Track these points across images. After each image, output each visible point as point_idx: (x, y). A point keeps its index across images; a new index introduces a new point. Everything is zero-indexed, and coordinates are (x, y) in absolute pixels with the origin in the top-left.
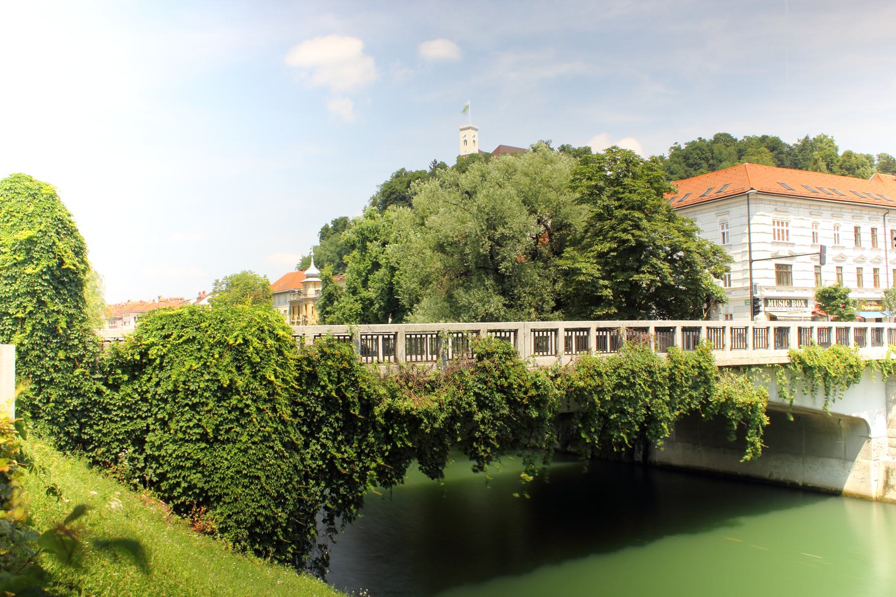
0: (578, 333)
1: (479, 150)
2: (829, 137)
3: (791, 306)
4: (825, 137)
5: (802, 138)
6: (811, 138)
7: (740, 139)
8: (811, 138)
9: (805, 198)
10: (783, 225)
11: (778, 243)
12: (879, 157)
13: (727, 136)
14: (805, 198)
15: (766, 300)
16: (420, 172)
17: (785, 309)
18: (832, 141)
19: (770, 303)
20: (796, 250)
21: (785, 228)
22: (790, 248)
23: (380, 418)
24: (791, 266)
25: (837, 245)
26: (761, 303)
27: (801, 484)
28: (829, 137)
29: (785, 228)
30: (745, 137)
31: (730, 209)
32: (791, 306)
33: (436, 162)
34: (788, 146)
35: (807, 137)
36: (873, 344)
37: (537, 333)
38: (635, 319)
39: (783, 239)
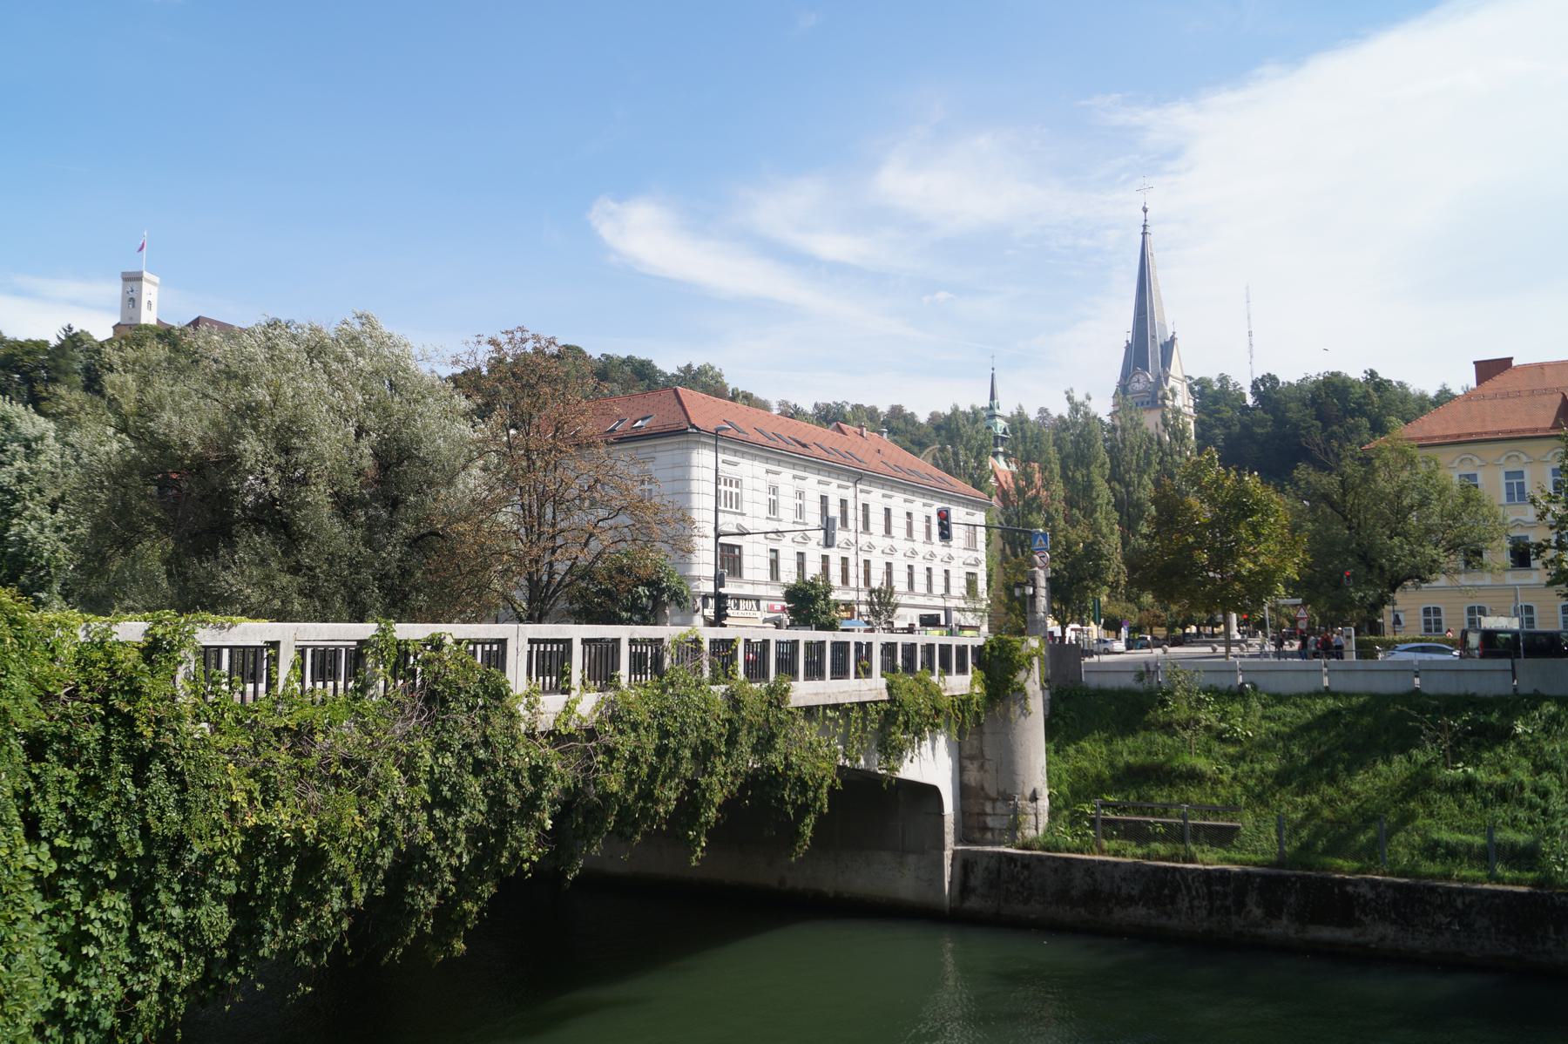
0: (542, 646)
1: (158, 321)
2: (717, 370)
3: (738, 609)
4: (712, 368)
5: (683, 365)
6: (695, 367)
7: (596, 356)
8: (695, 367)
9: (762, 447)
10: (731, 485)
11: (736, 513)
12: (780, 405)
13: (580, 351)
14: (762, 447)
15: (738, 598)
16: (36, 343)
17: (751, 614)
18: (720, 375)
19: (742, 603)
20: (748, 524)
21: (734, 490)
22: (739, 520)
23: (1507, 874)
24: (740, 547)
25: (798, 520)
26: (731, 603)
27: (831, 895)
28: (717, 370)
29: (734, 490)
30: (602, 355)
31: (656, 455)
32: (738, 609)
33: (70, 329)
34: (663, 374)
35: (689, 366)
36: (957, 672)
37: (542, 646)
38: (439, 622)
39: (731, 507)
